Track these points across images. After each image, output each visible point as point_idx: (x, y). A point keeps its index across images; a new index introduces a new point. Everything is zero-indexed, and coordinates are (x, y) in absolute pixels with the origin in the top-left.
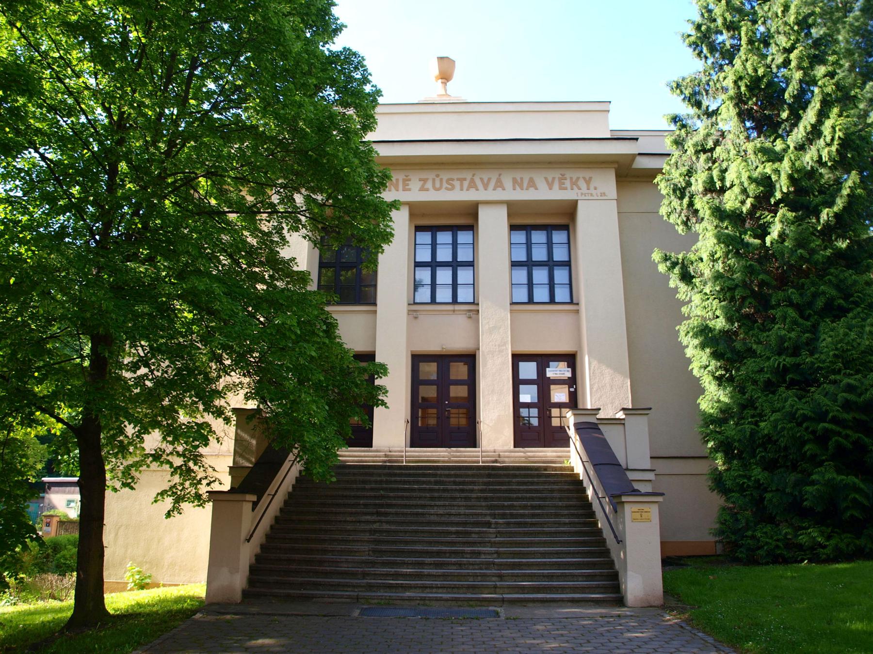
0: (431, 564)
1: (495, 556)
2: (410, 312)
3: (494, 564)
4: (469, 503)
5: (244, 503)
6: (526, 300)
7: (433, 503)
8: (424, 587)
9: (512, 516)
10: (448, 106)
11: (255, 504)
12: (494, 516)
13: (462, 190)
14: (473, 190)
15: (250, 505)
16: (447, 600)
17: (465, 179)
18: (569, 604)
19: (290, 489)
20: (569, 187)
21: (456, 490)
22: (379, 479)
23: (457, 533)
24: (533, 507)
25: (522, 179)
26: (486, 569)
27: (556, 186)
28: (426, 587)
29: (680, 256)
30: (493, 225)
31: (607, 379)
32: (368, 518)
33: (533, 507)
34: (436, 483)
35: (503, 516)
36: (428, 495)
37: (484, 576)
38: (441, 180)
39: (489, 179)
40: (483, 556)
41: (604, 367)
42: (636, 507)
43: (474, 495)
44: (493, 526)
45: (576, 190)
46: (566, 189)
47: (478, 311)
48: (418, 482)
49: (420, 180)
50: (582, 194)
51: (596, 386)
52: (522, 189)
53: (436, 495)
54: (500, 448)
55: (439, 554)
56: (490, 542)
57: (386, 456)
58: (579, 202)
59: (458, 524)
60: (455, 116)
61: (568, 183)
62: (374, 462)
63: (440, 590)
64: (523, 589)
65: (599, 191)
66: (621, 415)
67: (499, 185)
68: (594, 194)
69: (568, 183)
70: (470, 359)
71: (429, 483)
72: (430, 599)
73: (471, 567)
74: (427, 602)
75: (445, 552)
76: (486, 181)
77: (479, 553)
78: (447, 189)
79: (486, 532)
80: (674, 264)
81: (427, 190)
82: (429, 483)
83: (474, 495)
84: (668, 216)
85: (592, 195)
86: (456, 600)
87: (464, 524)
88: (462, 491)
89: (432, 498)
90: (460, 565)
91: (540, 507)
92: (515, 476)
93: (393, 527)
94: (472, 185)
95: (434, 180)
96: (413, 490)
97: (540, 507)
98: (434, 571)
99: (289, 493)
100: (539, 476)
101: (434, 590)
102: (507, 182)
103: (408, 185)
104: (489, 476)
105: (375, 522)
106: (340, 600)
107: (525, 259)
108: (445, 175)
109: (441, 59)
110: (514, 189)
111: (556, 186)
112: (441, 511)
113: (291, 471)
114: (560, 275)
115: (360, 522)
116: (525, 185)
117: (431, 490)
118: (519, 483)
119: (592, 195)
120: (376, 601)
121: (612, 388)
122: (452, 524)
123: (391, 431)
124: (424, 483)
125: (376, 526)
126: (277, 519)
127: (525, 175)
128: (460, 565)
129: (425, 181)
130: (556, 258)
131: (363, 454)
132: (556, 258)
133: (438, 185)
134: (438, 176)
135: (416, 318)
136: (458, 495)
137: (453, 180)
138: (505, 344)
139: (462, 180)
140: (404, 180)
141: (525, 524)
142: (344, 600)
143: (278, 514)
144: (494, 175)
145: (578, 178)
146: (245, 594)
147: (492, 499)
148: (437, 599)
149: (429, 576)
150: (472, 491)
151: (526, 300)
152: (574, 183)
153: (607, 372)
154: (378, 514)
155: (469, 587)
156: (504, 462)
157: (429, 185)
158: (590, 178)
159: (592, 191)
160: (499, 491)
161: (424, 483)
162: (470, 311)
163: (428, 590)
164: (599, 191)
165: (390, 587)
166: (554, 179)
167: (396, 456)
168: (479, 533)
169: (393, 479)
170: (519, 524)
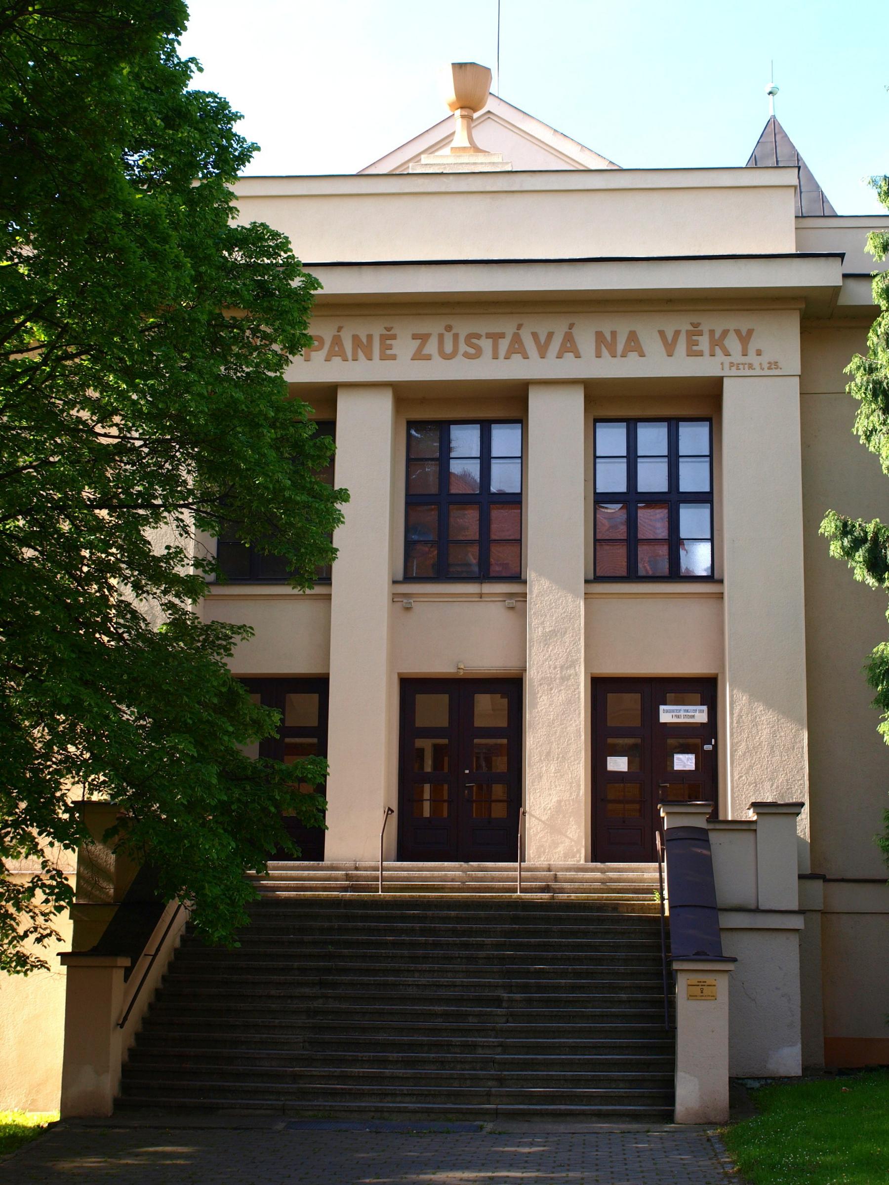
0: (397, 1061)
1: (499, 1050)
2: (395, 597)
3: (494, 1061)
4: (471, 967)
5: (114, 970)
6: (623, 572)
7: (412, 966)
8: (384, 1095)
9: (540, 988)
10: (471, 179)
11: (128, 971)
12: (509, 988)
13: (495, 357)
14: (517, 357)
15: (122, 973)
16: (414, 1112)
17: (502, 336)
18: (594, 1119)
19: (178, 943)
20: (707, 352)
21: (455, 944)
22: (326, 924)
23: (446, 1015)
24: (578, 975)
25: (614, 334)
26: (481, 1070)
27: (681, 346)
28: (387, 1095)
29: (870, 527)
30: (558, 420)
31: (765, 733)
32: (307, 991)
33: (578, 975)
34: (423, 932)
35: (525, 988)
36: (406, 952)
37: (475, 1079)
38: (456, 337)
39: (550, 335)
40: (480, 1051)
41: (760, 708)
42: (695, 978)
43: (482, 954)
44: (504, 1005)
45: (720, 356)
46: (700, 354)
47: (525, 595)
48: (392, 931)
49: (415, 337)
50: (732, 364)
51: (742, 748)
52: (614, 356)
53: (421, 952)
54: (561, 863)
55: (411, 1046)
56: (493, 1029)
57: (348, 877)
58: (725, 379)
59: (448, 1001)
60: (486, 201)
61: (704, 343)
62: (325, 889)
63: (408, 1099)
64: (530, 1098)
65: (765, 359)
66: (751, 815)
67: (569, 346)
68: (756, 365)
69: (704, 343)
70: (511, 688)
71: (412, 931)
72: (391, 1111)
73: (459, 1066)
74: (386, 1115)
75: (422, 1044)
76: (543, 339)
77: (474, 1046)
78: (467, 355)
79: (490, 1014)
80: (857, 543)
81: (428, 358)
82: (412, 931)
83: (482, 954)
84: (868, 438)
85: (751, 366)
86: (428, 1111)
87: (460, 1001)
88: (466, 946)
89: (413, 959)
90: (442, 1063)
91: (589, 974)
92: (559, 920)
93: (344, 1006)
94: (517, 348)
95: (441, 337)
96: (384, 945)
97: (589, 974)
98: (400, 1072)
99: (176, 950)
100: (601, 921)
101: (399, 1099)
102: (585, 340)
103: (390, 347)
104: (515, 920)
105: (316, 998)
106: (258, 1112)
107: (623, 489)
108: (464, 327)
109: (459, 67)
110: (598, 355)
111: (681, 346)
112: (423, 980)
113: (177, 915)
114: (692, 519)
115: (291, 997)
116: (620, 347)
117: (413, 945)
118: (563, 934)
119: (751, 366)
120: (310, 1113)
121: (772, 751)
122: (439, 1000)
123: (358, 827)
124: (403, 931)
125: (317, 1004)
126: (158, 994)
127: (621, 327)
128: (442, 1063)
129: (424, 338)
130: (686, 485)
131: (306, 873)
132: (686, 485)
133: (449, 348)
134: (449, 328)
135: (408, 609)
136: (456, 953)
137: (478, 336)
138: (573, 664)
139: (496, 337)
140: (383, 338)
141: (556, 1002)
142: (262, 1112)
143: (160, 985)
144: (559, 327)
145: (725, 333)
146: (119, 1104)
147: (512, 960)
148: (400, 1111)
149: (393, 1078)
150: (481, 946)
151: (623, 572)
152: (717, 342)
153: (766, 717)
154: (322, 984)
155: (449, 1095)
156: (562, 890)
157: (432, 347)
158: (750, 332)
159: (752, 358)
160: (528, 947)
161: (403, 931)
162: (511, 595)
163: (389, 1099)
164: (765, 359)
165: (334, 1094)
166: (677, 333)
167: (367, 879)
168: (479, 1015)
169: (350, 925)
170: (548, 1002)
